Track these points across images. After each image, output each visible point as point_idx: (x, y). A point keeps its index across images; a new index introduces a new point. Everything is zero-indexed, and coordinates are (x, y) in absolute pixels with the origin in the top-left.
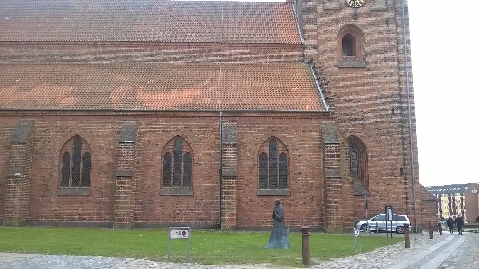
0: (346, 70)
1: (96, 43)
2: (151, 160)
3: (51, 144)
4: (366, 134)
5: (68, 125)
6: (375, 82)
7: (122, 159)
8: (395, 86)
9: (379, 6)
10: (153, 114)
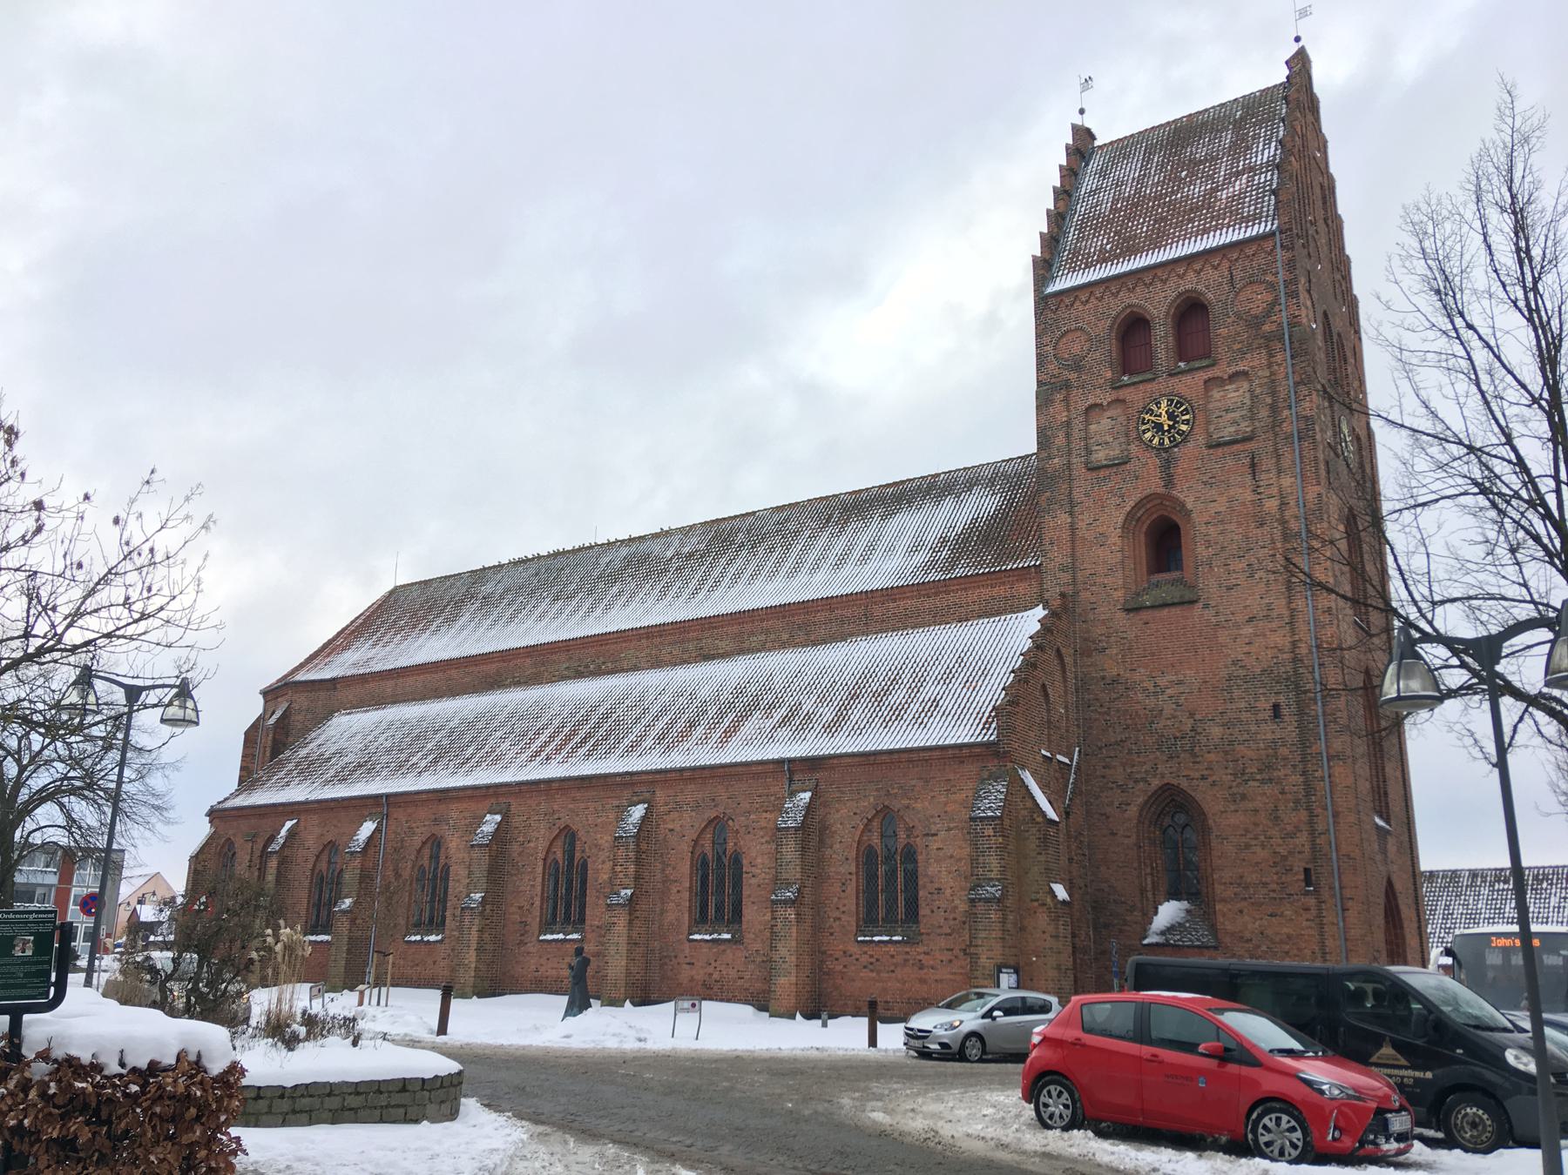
0: (1145, 615)
4: (1203, 778)
6: (1223, 636)
8: (1281, 639)
9: (1232, 429)
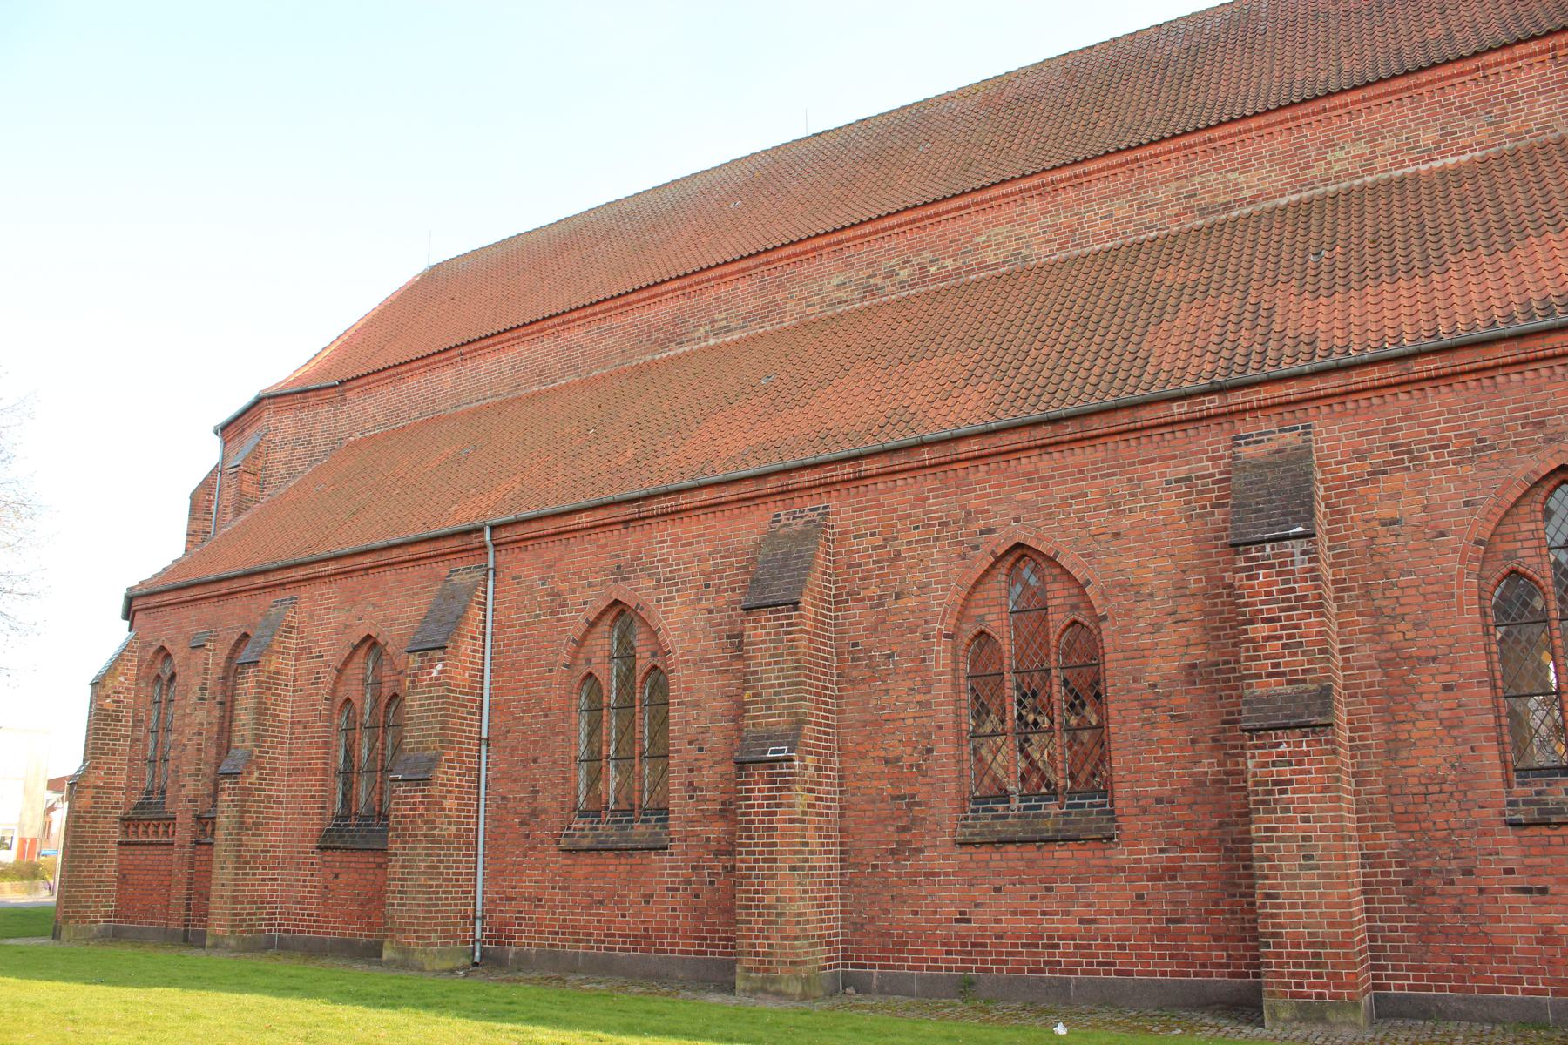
1: (1048, 178)
2: (1417, 626)
3: (911, 603)
5: (972, 503)
7: (1262, 630)
10: (1391, 372)
